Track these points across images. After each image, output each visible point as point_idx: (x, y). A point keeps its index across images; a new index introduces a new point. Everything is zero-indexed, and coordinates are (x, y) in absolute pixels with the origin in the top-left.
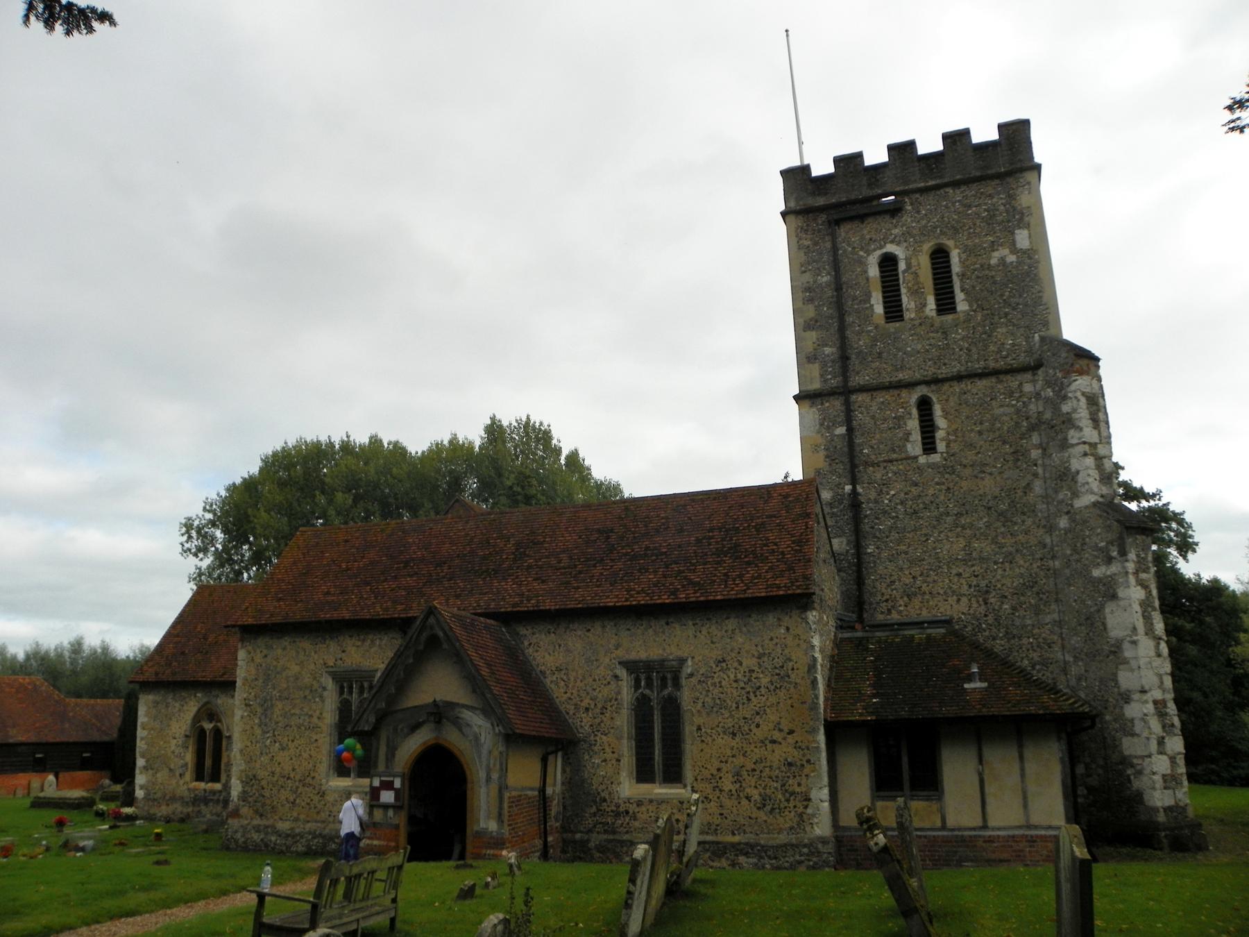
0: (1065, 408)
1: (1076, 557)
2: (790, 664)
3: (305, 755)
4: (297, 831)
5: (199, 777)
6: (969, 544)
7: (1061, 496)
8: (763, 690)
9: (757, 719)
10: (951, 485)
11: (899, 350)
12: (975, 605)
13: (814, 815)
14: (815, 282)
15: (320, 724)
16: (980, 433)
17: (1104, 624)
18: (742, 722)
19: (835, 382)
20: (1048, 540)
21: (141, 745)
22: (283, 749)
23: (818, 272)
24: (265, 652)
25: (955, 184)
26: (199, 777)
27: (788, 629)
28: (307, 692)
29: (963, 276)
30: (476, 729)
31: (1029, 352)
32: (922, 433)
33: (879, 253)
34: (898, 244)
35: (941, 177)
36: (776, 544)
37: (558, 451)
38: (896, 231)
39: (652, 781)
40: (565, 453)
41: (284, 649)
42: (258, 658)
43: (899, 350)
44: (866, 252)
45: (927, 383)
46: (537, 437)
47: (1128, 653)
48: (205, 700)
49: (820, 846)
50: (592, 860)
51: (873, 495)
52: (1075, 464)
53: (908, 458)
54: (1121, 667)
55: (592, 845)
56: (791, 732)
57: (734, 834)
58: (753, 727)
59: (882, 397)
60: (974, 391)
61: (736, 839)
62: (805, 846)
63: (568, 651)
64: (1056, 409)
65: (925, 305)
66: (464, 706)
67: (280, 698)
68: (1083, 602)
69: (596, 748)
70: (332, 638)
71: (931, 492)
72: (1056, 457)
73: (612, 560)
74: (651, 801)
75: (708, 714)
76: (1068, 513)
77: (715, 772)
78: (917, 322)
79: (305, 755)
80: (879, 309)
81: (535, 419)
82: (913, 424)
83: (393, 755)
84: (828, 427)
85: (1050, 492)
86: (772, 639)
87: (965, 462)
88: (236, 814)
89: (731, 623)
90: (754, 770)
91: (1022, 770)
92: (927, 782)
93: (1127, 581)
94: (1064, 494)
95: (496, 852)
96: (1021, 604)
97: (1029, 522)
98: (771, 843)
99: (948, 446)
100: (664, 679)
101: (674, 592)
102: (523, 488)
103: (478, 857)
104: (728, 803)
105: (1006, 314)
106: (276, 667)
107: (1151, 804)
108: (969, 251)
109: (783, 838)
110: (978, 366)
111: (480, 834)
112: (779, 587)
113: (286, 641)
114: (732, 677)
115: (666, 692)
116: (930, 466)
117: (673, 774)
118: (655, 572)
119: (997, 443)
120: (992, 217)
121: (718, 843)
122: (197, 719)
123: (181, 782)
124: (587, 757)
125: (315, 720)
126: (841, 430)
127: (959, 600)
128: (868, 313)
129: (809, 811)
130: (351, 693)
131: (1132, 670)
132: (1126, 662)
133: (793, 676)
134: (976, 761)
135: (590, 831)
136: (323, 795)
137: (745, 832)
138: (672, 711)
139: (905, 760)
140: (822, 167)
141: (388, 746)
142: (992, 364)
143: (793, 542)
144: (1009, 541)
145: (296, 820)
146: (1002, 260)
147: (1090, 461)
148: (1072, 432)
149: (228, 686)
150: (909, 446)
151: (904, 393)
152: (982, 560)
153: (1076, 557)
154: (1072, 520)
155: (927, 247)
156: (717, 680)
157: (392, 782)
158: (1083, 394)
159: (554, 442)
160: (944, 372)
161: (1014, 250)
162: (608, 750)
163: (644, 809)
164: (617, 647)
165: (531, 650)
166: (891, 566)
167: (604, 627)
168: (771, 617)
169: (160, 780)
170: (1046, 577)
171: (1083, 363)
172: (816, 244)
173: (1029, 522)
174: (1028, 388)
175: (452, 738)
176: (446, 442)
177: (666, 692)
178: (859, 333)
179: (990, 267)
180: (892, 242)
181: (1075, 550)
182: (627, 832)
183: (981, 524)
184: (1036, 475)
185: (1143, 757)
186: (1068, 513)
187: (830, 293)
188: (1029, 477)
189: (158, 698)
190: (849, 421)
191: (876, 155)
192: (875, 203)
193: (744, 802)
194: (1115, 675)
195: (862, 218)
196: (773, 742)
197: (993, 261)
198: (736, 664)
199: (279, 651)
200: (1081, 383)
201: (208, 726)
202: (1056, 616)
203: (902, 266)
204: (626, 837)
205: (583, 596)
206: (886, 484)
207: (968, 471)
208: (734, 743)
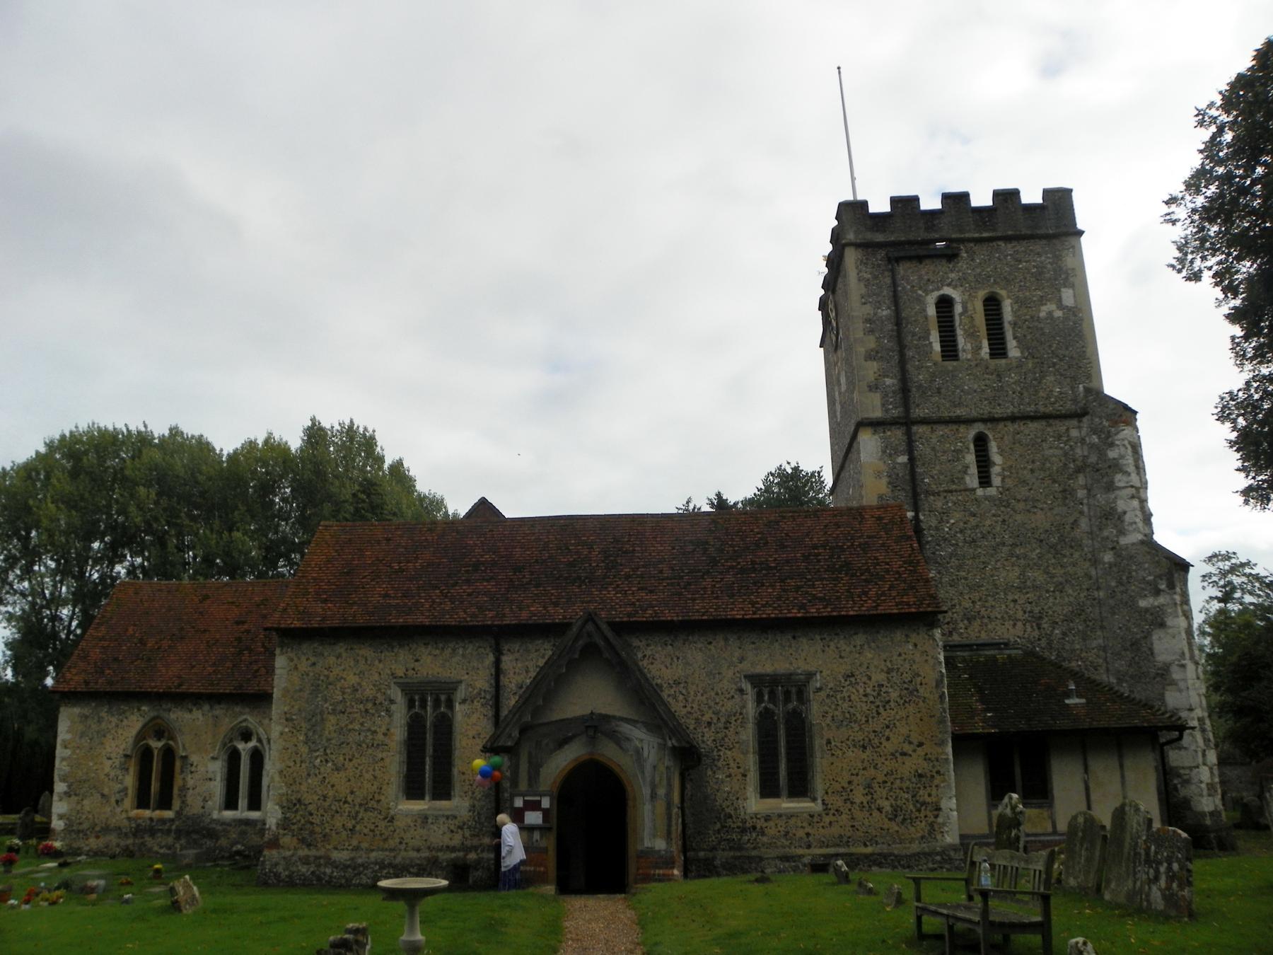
0: (1112, 454)
1: (1122, 588)
2: (919, 680)
3: (367, 776)
4: (360, 861)
6: (1023, 573)
7: (1106, 533)
8: (892, 704)
9: (887, 732)
10: (1006, 518)
11: (957, 387)
12: (1029, 629)
13: (944, 824)
14: (875, 314)
15: (387, 741)
16: (1032, 471)
17: (1151, 650)
18: (872, 736)
19: (896, 413)
20: (1093, 573)
21: (60, 766)
22: (338, 769)
23: (878, 305)
24: (313, 659)
25: (1007, 239)
27: (915, 645)
28: (369, 705)
29: (1014, 325)
30: (638, 744)
31: (1075, 401)
32: (978, 467)
33: (936, 294)
34: (955, 287)
35: (994, 230)
36: (887, 564)
37: (381, 459)
38: (952, 275)
40: (388, 462)
42: (304, 665)
43: (957, 387)
44: (927, 289)
45: (984, 421)
46: (359, 444)
47: (1176, 674)
48: (152, 714)
49: (952, 853)
50: (719, 875)
51: (934, 523)
52: (1121, 505)
53: (966, 490)
54: (1169, 688)
55: (717, 862)
56: (921, 744)
57: (866, 845)
58: (883, 740)
59: (942, 430)
60: (1027, 432)
61: (869, 850)
62: (937, 854)
63: (687, 663)
64: (1102, 455)
65: (980, 348)
66: (622, 719)
67: (334, 712)
68: (1128, 629)
69: (720, 764)
70: (401, 646)
71: (988, 522)
72: (1101, 498)
73: (721, 573)
74: (780, 816)
75: (838, 728)
76: (1113, 548)
77: (846, 785)
78: (973, 363)
79: (367, 776)
80: (937, 347)
81: (360, 423)
82: (971, 458)
83: (538, 773)
84: (890, 455)
85: (1095, 529)
86: (900, 655)
87: (1019, 497)
88: (274, 843)
89: (859, 639)
90: (885, 782)
91: (1123, 777)
92: (1039, 792)
93: (1176, 612)
94: (1109, 532)
95: (666, 872)
96: (1070, 629)
97: (1076, 555)
98: (904, 852)
99: (1003, 481)
100: (787, 694)
101: (803, 606)
102: (368, 496)
103: (648, 879)
104: (858, 814)
105: (1054, 364)
106: (328, 677)
107: (1199, 809)
108: (1020, 303)
109: (915, 848)
110: (1030, 409)
111: (650, 852)
112: (908, 604)
113: (341, 648)
114: (861, 691)
115: (790, 706)
116: (987, 498)
117: (800, 788)
118: (773, 586)
119: (1048, 482)
120: (1041, 273)
121: (852, 854)
122: (141, 736)
124: (710, 773)
125: (380, 737)
126: (903, 459)
127: (1014, 625)
128: (926, 351)
129: (940, 820)
130: (423, 705)
131: (1180, 691)
132: (1173, 683)
133: (921, 691)
134: (1081, 769)
135: (714, 849)
136: (392, 820)
137: (877, 843)
138: (799, 729)
139: (1018, 770)
140: (879, 205)
141: (530, 762)
142: (1042, 409)
143: (905, 562)
144: (1059, 571)
145: (357, 849)
146: (1050, 313)
147: (1135, 503)
148: (1118, 477)
149: (261, 699)
150: (967, 479)
151: (962, 428)
152: (1035, 588)
153: (1122, 588)
154: (1118, 555)
155: (982, 294)
156: (846, 694)
157: (540, 802)
158: (1130, 443)
159: (378, 449)
160: (998, 412)
161: (1060, 306)
162: (732, 764)
163: (772, 824)
164: (742, 660)
165: (645, 662)
166: (952, 591)
167: (726, 640)
168: (898, 634)
169: (87, 808)
170: (1092, 606)
171: (1128, 414)
172: (876, 277)
173: (1076, 555)
174: (1074, 433)
175: (609, 752)
176: (260, 442)
177: (790, 706)
178: (918, 368)
179: (1039, 320)
180: (949, 285)
181: (1120, 583)
182: (754, 848)
183: (1034, 555)
184: (1081, 513)
185: (1191, 768)
186: (1113, 548)
187: (890, 327)
188: (1076, 515)
189: (86, 711)
190: (910, 450)
191: (981, 198)
192: (932, 246)
193: (876, 813)
194: (1163, 695)
195: (920, 259)
196: (904, 754)
197: (1042, 314)
198: (865, 679)
199: (332, 660)
200: (1127, 432)
201: (156, 745)
202: (1101, 641)
203: (958, 309)
204: (754, 853)
205: (700, 609)
206: (946, 513)
207: (1021, 506)
208: (864, 756)
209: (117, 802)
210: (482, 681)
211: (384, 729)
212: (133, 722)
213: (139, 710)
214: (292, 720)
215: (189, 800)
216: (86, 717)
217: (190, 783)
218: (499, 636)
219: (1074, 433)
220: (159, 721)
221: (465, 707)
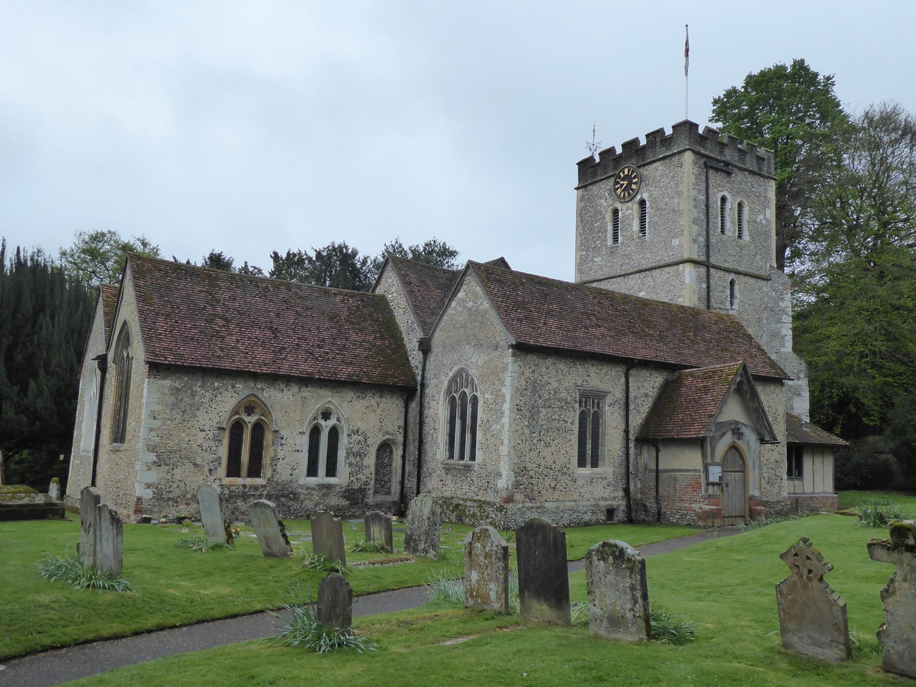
5: (233, 470)
24: (533, 368)
39: (238, 475)
41: (547, 368)
42: (528, 372)
48: (247, 392)
66: (745, 425)
113: (550, 361)
125: (569, 425)
126: (704, 286)
155: (738, 200)
199: (544, 369)
209: (210, 471)
210: (619, 393)
211: (571, 420)
212: (225, 401)
213: (233, 387)
214: (521, 410)
215: (279, 468)
216: (178, 390)
217: (280, 454)
218: (630, 364)
219: (765, 289)
220: (253, 398)
221: (611, 408)
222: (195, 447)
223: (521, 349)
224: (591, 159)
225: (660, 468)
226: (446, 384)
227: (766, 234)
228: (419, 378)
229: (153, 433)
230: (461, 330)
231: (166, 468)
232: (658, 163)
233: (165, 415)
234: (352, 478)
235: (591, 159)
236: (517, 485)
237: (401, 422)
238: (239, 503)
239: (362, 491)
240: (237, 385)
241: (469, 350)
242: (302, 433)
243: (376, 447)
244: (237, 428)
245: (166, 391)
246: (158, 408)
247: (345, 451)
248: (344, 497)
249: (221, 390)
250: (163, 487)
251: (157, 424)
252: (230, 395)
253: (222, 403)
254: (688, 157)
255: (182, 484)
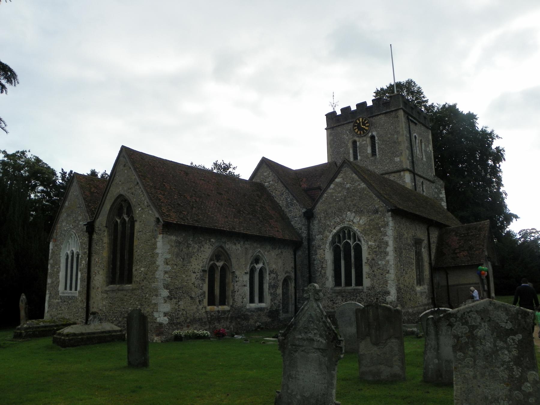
5: (211, 302)
26: (211, 302)
123: (200, 307)
126: (413, 184)
189: (180, 239)
209: (200, 301)
213: (210, 241)
216: (180, 243)
222: (191, 285)
223: (397, 213)
224: (334, 113)
225: (449, 284)
226: (330, 238)
227: (431, 159)
228: (304, 235)
229: (167, 275)
230: (342, 203)
231: (175, 300)
232: (381, 116)
233: (173, 262)
234: (272, 303)
235: (334, 113)
236: (398, 298)
237: (292, 265)
238: (216, 324)
239: (277, 311)
240: (212, 240)
241: (350, 215)
242: (246, 273)
243: (282, 281)
244: (212, 270)
245: (173, 244)
246: (169, 256)
247: (268, 285)
248: (269, 316)
249: (203, 243)
250: (174, 315)
251: (169, 268)
252: (208, 247)
253: (203, 253)
254: (401, 113)
255: (184, 313)
